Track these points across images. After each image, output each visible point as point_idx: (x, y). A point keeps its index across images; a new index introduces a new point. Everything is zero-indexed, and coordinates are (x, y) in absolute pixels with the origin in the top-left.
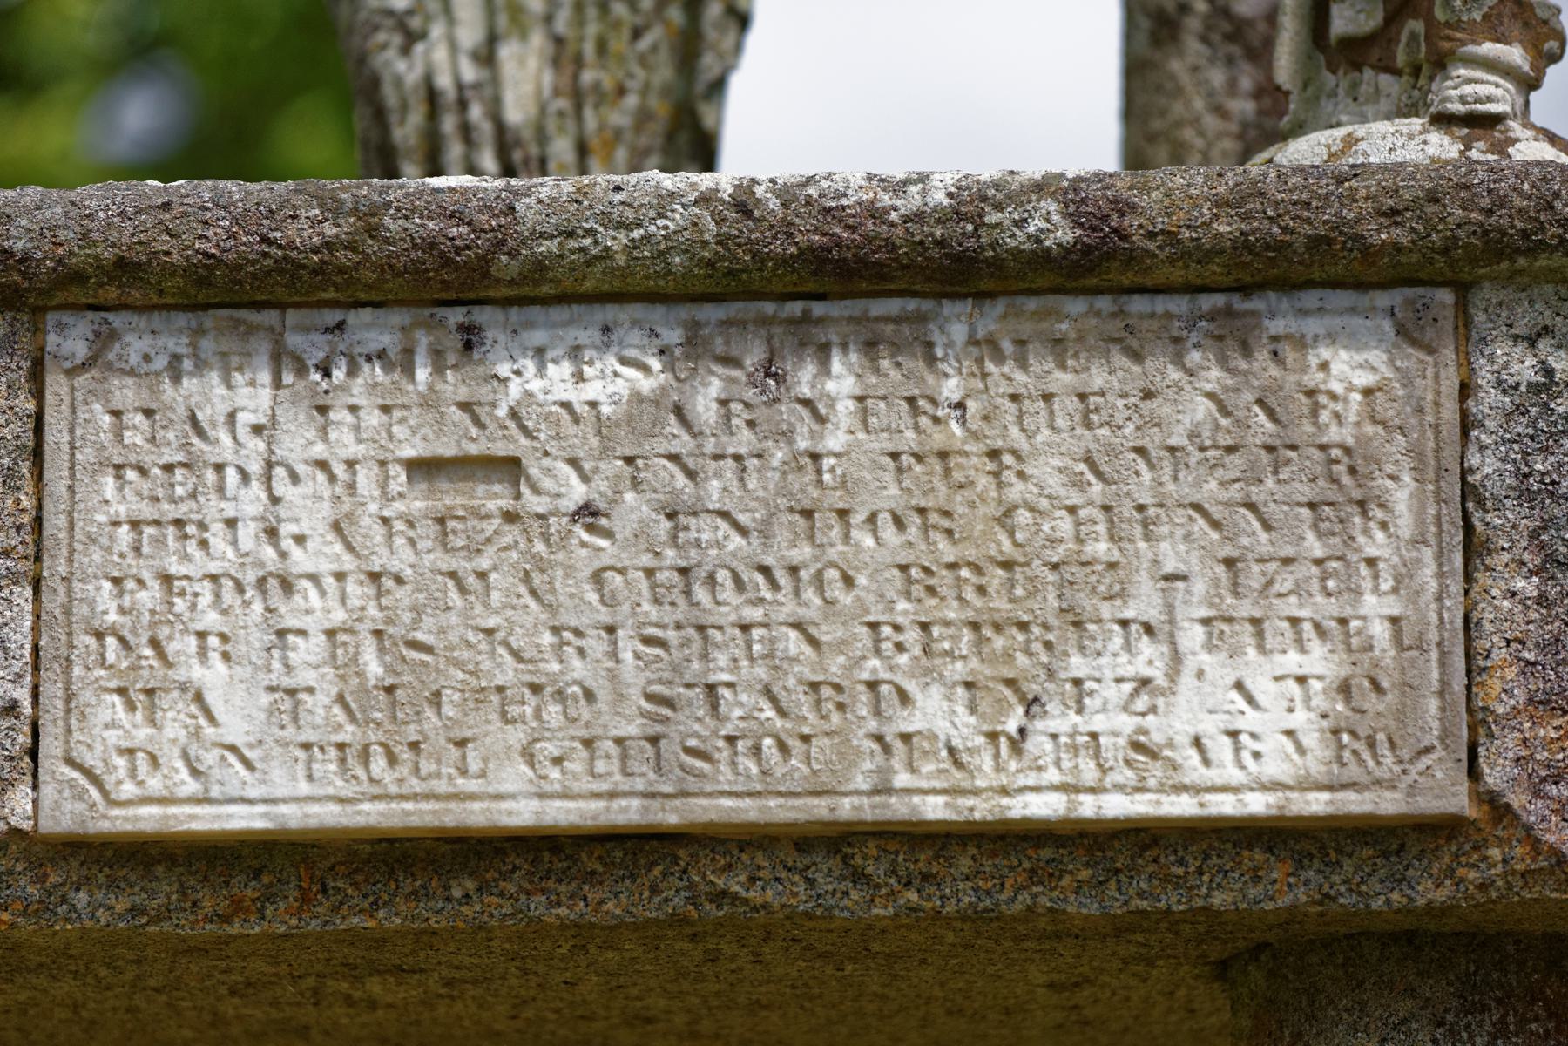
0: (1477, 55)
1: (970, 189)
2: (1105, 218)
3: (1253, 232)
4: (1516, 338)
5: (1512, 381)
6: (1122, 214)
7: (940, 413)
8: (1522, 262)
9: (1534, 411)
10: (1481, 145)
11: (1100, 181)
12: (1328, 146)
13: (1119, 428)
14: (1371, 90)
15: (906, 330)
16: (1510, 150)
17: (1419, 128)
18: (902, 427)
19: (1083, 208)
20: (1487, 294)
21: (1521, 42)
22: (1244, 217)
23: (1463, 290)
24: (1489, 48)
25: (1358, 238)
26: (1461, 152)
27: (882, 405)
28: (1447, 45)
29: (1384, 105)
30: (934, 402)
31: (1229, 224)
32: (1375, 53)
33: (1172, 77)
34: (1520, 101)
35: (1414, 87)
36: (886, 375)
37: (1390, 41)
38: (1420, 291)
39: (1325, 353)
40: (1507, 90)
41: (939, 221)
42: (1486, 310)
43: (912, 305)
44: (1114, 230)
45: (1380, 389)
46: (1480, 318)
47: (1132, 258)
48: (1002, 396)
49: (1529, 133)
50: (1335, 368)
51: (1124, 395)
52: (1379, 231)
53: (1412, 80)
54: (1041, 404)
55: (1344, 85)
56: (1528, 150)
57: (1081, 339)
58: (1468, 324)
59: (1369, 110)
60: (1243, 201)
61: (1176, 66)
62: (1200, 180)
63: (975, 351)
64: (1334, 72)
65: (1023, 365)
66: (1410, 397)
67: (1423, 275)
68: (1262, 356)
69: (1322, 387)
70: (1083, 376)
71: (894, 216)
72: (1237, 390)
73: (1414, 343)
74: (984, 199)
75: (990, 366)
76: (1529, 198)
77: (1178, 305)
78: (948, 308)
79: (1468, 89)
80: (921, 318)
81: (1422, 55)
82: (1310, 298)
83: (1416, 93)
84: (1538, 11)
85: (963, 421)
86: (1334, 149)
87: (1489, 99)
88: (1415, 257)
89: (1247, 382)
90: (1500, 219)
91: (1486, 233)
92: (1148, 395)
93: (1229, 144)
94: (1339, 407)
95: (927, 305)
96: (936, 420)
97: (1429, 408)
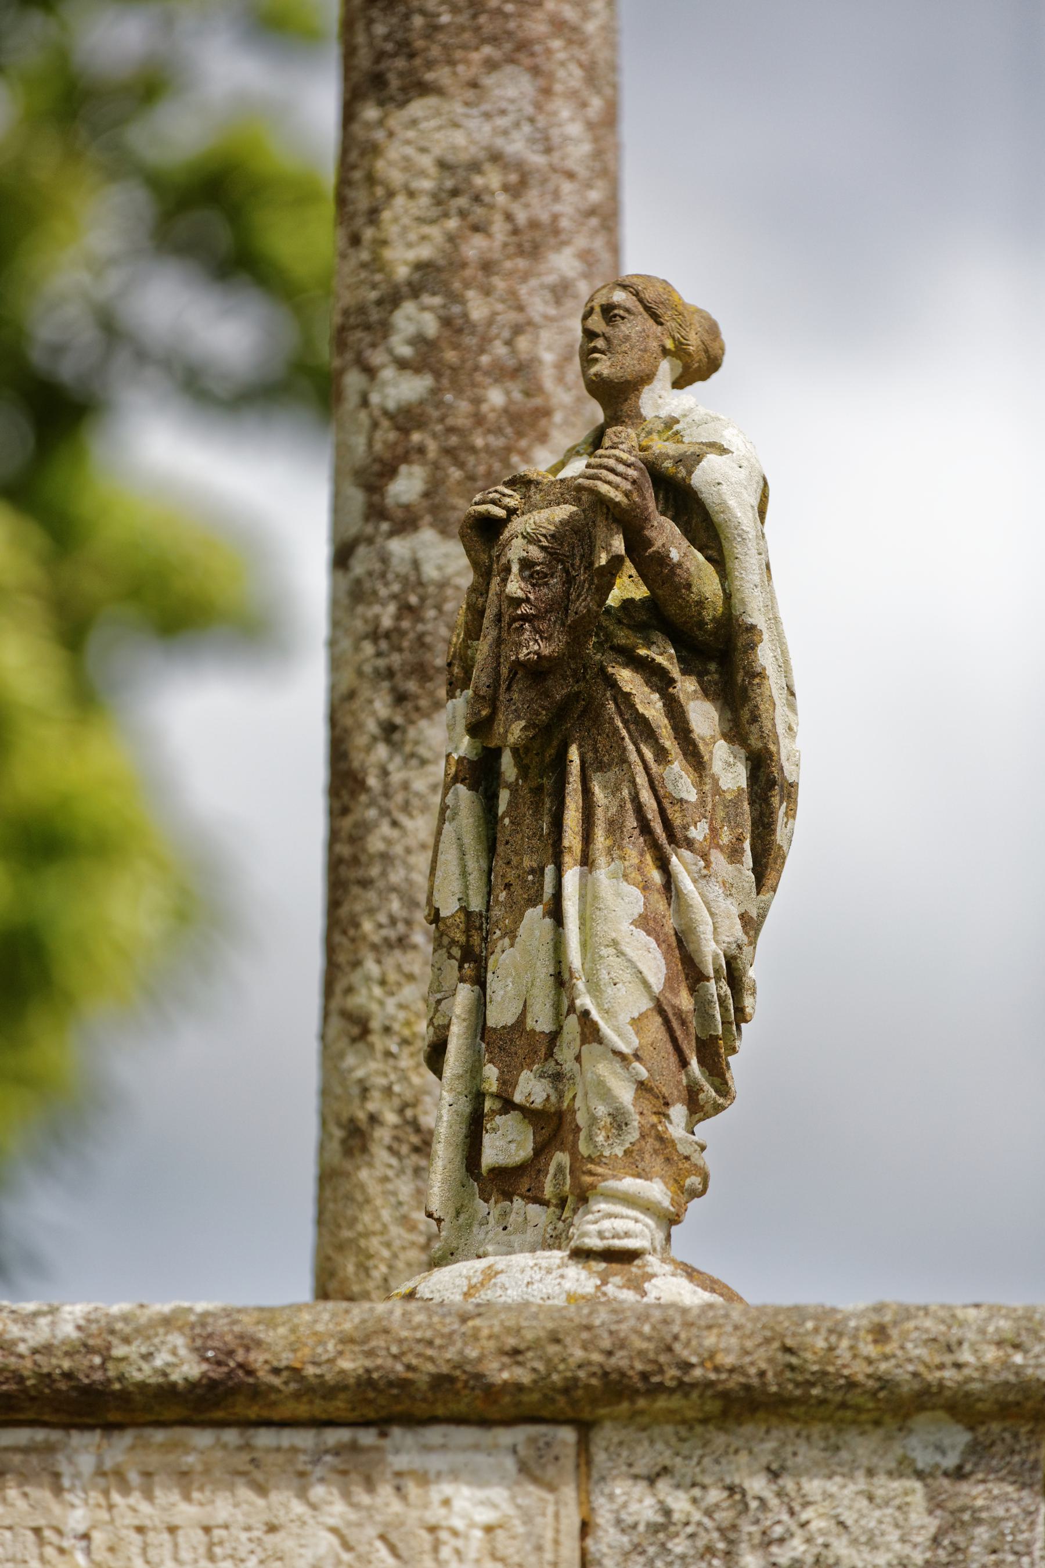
0: (617, 1190)
1: (97, 1321)
2: (231, 1353)
3: (378, 1368)
4: (636, 1477)
5: (630, 1520)
6: (248, 1349)
7: (66, 1544)
8: (641, 1403)
9: (651, 1550)
10: (617, 1280)
11: (228, 1316)
12: (469, 1278)
13: (242, 1561)
14: (520, 1219)
15: (34, 1460)
16: (646, 1285)
17: (558, 1261)
18: (28, 1558)
19: (210, 1343)
20: (606, 1436)
21: (662, 1177)
22: (370, 1354)
23: (585, 1428)
24: (629, 1184)
25: (479, 1376)
26: (598, 1287)
27: (8, 1534)
28: (587, 1179)
29: (531, 1235)
30: (59, 1532)
31: (354, 1360)
32: (525, 1184)
33: (362, 1187)
34: (660, 1236)
35: (559, 1219)
36: (13, 1505)
37: (539, 1171)
38: (542, 1429)
39: (447, 1489)
40: (647, 1226)
41: (67, 1354)
42: (606, 1449)
43: (40, 1435)
44: (240, 1366)
45: (501, 1526)
46: (600, 1457)
47: (257, 1393)
48: (127, 1527)
49: (668, 1268)
50: (458, 1504)
51: (248, 1528)
52: (501, 1370)
53: (558, 1211)
54: (166, 1536)
55: (496, 1212)
56: (669, 1288)
57: (207, 1471)
58: (589, 1463)
59: (516, 1240)
60: (367, 1339)
61: (364, 1174)
62: (326, 1316)
63: (101, 1481)
64: (487, 1201)
65: (149, 1495)
66: (529, 1535)
67: (545, 1413)
68: (385, 1491)
69: (444, 1523)
70: (209, 1508)
71: (22, 1348)
72: (359, 1525)
73: (536, 1480)
74: (112, 1332)
75: (116, 1497)
76: (649, 1339)
77: (304, 1439)
78: (77, 1438)
79: (606, 1224)
80: (50, 1449)
81: (567, 1188)
82: (434, 1434)
83: (560, 1225)
84: (679, 1147)
85: (88, 1552)
86: (474, 1281)
87: (627, 1235)
88: (536, 1397)
89: (371, 1517)
90: (620, 1360)
91: (606, 1374)
92: (272, 1529)
93: (414, 1255)
94: (459, 1543)
95: (55, 1435)
96: (62, 1551)
97: (548, 1545)
